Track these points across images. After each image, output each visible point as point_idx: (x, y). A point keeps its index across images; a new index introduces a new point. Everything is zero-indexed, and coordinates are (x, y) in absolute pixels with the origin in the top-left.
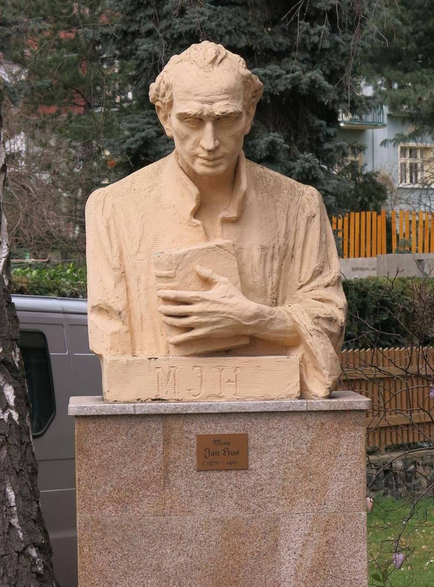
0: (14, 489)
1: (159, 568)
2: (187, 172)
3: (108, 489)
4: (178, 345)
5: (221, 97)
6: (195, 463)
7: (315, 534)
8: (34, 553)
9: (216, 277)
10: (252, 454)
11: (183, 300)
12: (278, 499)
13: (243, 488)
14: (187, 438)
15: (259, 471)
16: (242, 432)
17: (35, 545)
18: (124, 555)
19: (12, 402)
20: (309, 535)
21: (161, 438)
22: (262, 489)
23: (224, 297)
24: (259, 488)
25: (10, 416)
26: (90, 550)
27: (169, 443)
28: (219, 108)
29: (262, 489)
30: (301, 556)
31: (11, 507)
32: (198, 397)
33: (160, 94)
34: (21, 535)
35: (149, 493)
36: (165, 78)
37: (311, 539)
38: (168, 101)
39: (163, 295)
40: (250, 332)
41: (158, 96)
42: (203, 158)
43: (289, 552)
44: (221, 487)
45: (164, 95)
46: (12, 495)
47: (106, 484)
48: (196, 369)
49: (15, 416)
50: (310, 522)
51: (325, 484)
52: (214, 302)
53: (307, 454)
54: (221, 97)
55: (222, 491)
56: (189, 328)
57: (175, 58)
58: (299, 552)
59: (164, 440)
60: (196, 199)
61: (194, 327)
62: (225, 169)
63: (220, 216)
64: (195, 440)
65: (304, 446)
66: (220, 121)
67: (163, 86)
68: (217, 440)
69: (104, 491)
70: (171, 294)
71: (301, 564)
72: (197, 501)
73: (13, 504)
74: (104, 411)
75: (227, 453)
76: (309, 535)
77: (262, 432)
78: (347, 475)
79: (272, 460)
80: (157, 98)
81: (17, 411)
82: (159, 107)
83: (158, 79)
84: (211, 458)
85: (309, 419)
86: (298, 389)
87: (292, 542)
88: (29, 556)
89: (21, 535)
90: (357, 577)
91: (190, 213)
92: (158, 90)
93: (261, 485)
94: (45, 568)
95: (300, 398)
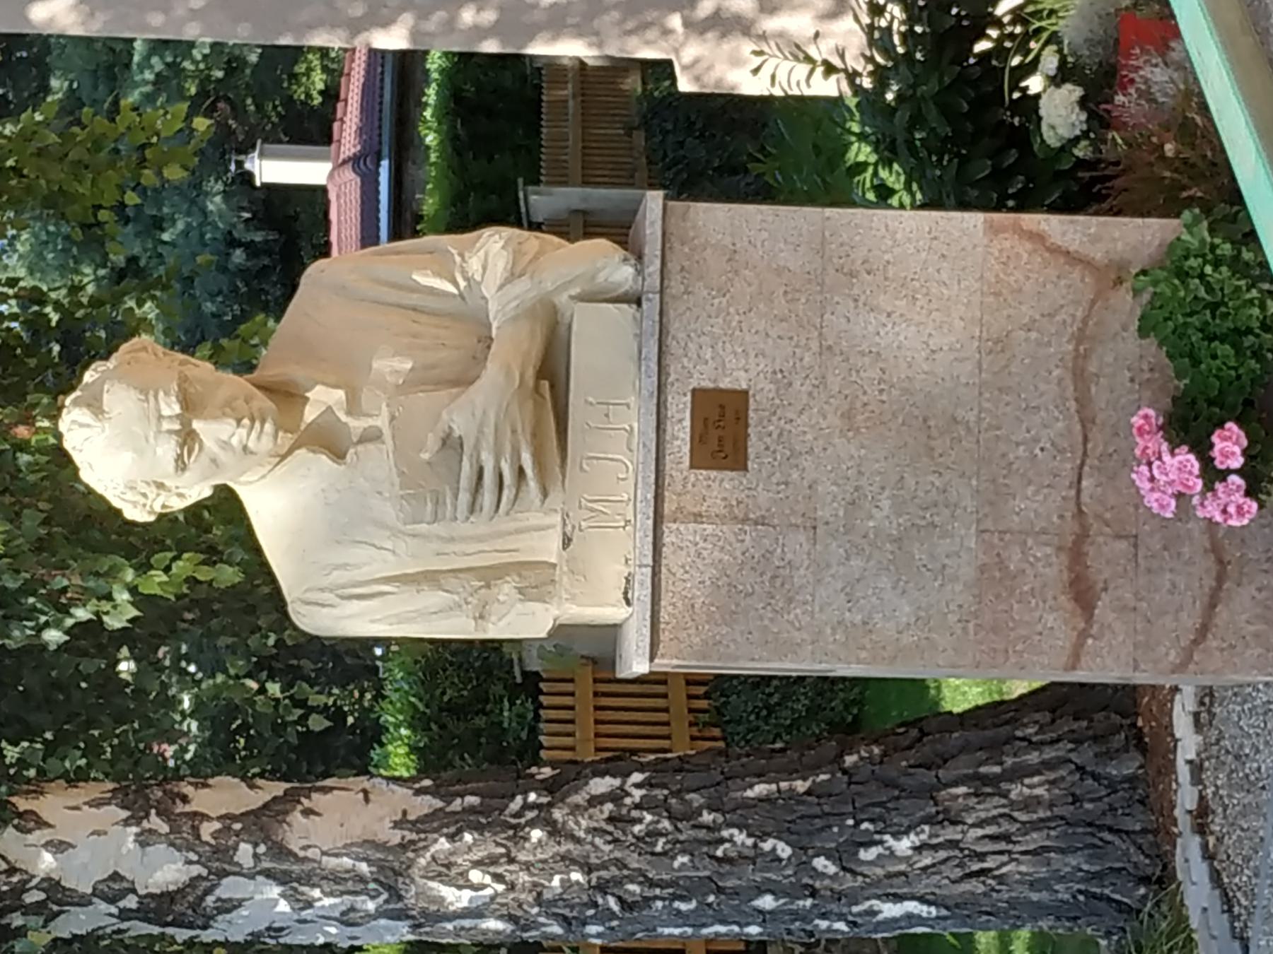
0: (751, 786)
1: (898, 540)
2: (270, 467)
3: (770, 615)
4: (545, 494)
5: (151, 399)
6: (734, 474)
7: (856, 291)
8: (850, 760)
9: (441, 429)
10: (725, 384)
11: (475, 478)
12: (797, 346)
13: (777, 401)
14: (694, 486)
15: (753, 374)
16: (689, 397)
17: (841, 756)
18: (874, 594)
19: (617, 782)
20: (856, 300)
21: (692, 526)
22: (781, 371)
23: (473, 415)
24: (779, 376)
25: (638, 786)
26: (863, 648)
27: (701, 516)
28: (171, 407)
29: (781, 371)
30: (889, 315)
31: (779, 791)
32: (629, 464)
33: (143, 500)
34: (823, 777)
35: (779, 550)
36: (117, 492)
37: (863, 298)
38: (154, 489)
39: (466, 513)
40: (530, 373)
41: (144, 505)
42: (249, 435)
43: (882, 333)
44: (775, 436)
45: (144, 495)
46: (760, 789)
47: (761, 618)
48: (585, 466)
49: (637, 777)
50: (836, 299)
51: (779, 271)
52: (481, 431)
53: (728, 296)
54: (151, 399)
55: (780, 435)
56: (521, 472)
57: (85, 475)
58: (883, 318)
59: (695, 522)
60: (314, 452)
61: (516, 467)
62: (373, 31)
63: (343, 418)
64: (698, 472)
65: (716, 301)
66: (190, 405)
67: (129, 496)
68: (698, 439)
69: (772, 620)
70: (464, 497)
71: (902, 315)
72: (795, 475)
73: (774, 787)
74: (644, 615)
75: (721, 424)
76: (856, 300)
77: (691, 366)
78: (765, 235)
79: (735, 353)
80: (148, 508)
81: (628, 775)
82: (164, 506)
83: (116, 503)
84: (728, 448)
85: (674, 291)
86: (625, 306)
87: (866, 328)
88: (855, 765)
89: (823, 777)
90: (927, 229)
91: (335, 465)
92: (135, 504)
93: (774, 372)
94: (876, 742)
95: (639, 303)
